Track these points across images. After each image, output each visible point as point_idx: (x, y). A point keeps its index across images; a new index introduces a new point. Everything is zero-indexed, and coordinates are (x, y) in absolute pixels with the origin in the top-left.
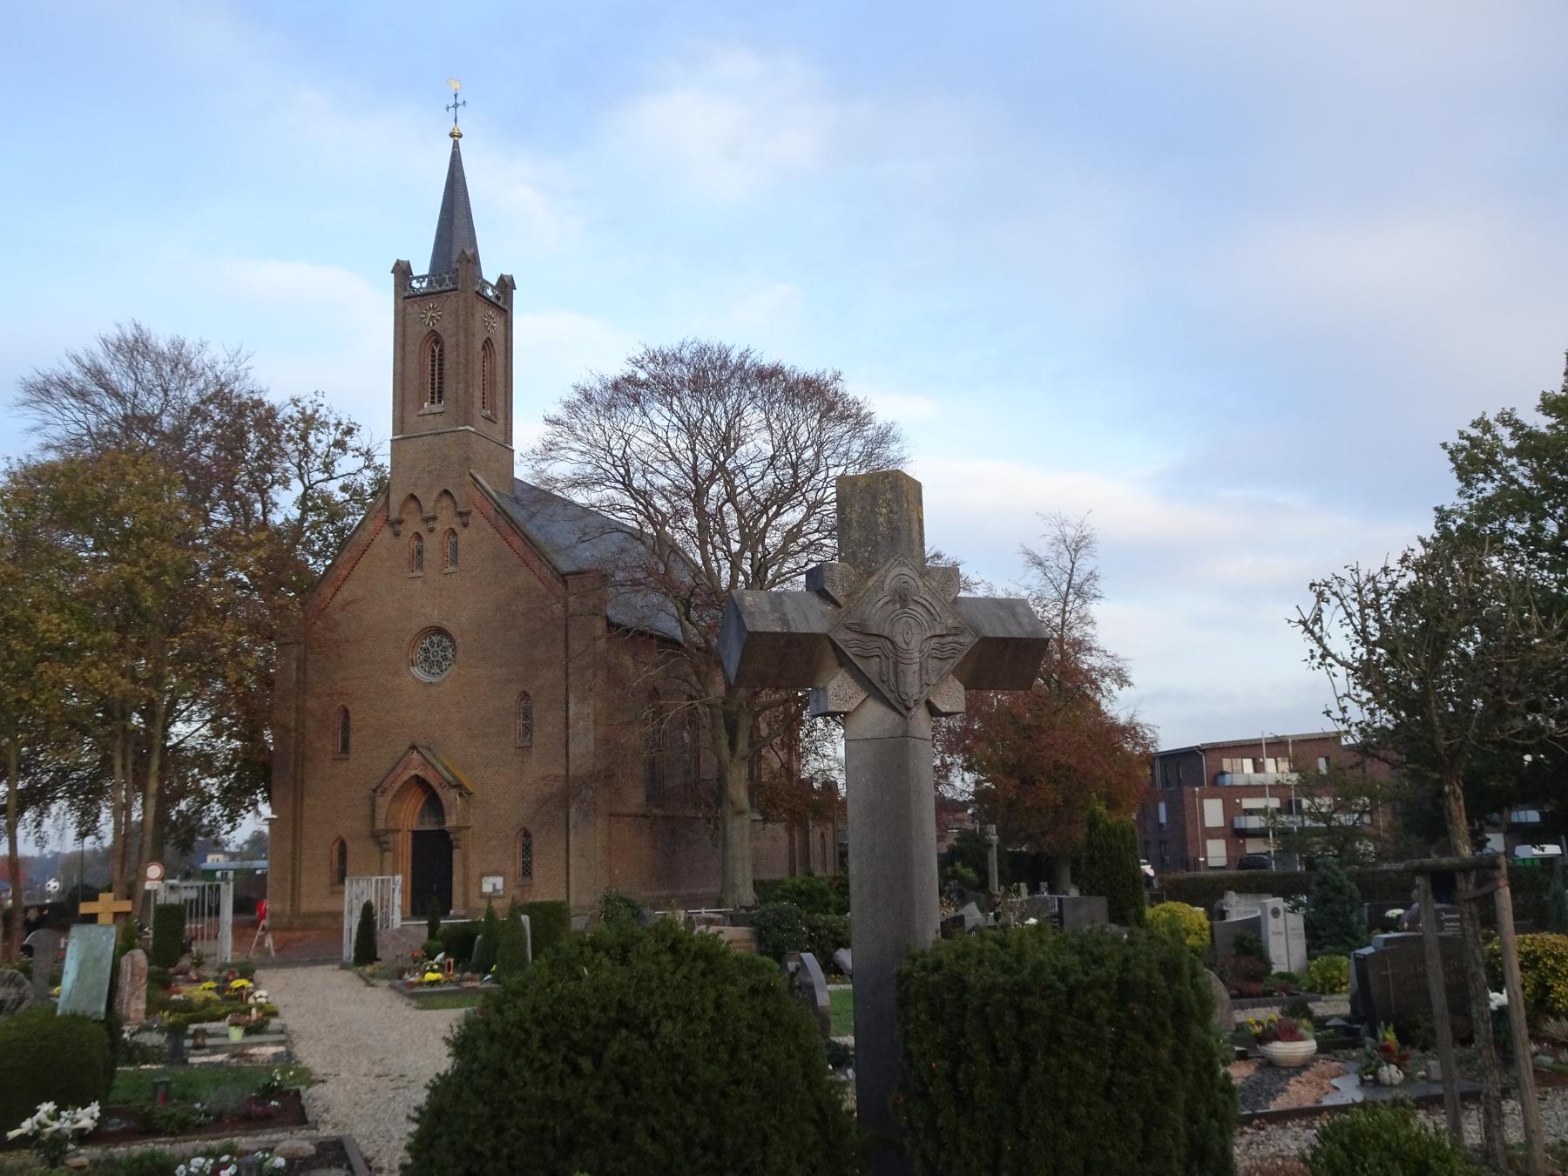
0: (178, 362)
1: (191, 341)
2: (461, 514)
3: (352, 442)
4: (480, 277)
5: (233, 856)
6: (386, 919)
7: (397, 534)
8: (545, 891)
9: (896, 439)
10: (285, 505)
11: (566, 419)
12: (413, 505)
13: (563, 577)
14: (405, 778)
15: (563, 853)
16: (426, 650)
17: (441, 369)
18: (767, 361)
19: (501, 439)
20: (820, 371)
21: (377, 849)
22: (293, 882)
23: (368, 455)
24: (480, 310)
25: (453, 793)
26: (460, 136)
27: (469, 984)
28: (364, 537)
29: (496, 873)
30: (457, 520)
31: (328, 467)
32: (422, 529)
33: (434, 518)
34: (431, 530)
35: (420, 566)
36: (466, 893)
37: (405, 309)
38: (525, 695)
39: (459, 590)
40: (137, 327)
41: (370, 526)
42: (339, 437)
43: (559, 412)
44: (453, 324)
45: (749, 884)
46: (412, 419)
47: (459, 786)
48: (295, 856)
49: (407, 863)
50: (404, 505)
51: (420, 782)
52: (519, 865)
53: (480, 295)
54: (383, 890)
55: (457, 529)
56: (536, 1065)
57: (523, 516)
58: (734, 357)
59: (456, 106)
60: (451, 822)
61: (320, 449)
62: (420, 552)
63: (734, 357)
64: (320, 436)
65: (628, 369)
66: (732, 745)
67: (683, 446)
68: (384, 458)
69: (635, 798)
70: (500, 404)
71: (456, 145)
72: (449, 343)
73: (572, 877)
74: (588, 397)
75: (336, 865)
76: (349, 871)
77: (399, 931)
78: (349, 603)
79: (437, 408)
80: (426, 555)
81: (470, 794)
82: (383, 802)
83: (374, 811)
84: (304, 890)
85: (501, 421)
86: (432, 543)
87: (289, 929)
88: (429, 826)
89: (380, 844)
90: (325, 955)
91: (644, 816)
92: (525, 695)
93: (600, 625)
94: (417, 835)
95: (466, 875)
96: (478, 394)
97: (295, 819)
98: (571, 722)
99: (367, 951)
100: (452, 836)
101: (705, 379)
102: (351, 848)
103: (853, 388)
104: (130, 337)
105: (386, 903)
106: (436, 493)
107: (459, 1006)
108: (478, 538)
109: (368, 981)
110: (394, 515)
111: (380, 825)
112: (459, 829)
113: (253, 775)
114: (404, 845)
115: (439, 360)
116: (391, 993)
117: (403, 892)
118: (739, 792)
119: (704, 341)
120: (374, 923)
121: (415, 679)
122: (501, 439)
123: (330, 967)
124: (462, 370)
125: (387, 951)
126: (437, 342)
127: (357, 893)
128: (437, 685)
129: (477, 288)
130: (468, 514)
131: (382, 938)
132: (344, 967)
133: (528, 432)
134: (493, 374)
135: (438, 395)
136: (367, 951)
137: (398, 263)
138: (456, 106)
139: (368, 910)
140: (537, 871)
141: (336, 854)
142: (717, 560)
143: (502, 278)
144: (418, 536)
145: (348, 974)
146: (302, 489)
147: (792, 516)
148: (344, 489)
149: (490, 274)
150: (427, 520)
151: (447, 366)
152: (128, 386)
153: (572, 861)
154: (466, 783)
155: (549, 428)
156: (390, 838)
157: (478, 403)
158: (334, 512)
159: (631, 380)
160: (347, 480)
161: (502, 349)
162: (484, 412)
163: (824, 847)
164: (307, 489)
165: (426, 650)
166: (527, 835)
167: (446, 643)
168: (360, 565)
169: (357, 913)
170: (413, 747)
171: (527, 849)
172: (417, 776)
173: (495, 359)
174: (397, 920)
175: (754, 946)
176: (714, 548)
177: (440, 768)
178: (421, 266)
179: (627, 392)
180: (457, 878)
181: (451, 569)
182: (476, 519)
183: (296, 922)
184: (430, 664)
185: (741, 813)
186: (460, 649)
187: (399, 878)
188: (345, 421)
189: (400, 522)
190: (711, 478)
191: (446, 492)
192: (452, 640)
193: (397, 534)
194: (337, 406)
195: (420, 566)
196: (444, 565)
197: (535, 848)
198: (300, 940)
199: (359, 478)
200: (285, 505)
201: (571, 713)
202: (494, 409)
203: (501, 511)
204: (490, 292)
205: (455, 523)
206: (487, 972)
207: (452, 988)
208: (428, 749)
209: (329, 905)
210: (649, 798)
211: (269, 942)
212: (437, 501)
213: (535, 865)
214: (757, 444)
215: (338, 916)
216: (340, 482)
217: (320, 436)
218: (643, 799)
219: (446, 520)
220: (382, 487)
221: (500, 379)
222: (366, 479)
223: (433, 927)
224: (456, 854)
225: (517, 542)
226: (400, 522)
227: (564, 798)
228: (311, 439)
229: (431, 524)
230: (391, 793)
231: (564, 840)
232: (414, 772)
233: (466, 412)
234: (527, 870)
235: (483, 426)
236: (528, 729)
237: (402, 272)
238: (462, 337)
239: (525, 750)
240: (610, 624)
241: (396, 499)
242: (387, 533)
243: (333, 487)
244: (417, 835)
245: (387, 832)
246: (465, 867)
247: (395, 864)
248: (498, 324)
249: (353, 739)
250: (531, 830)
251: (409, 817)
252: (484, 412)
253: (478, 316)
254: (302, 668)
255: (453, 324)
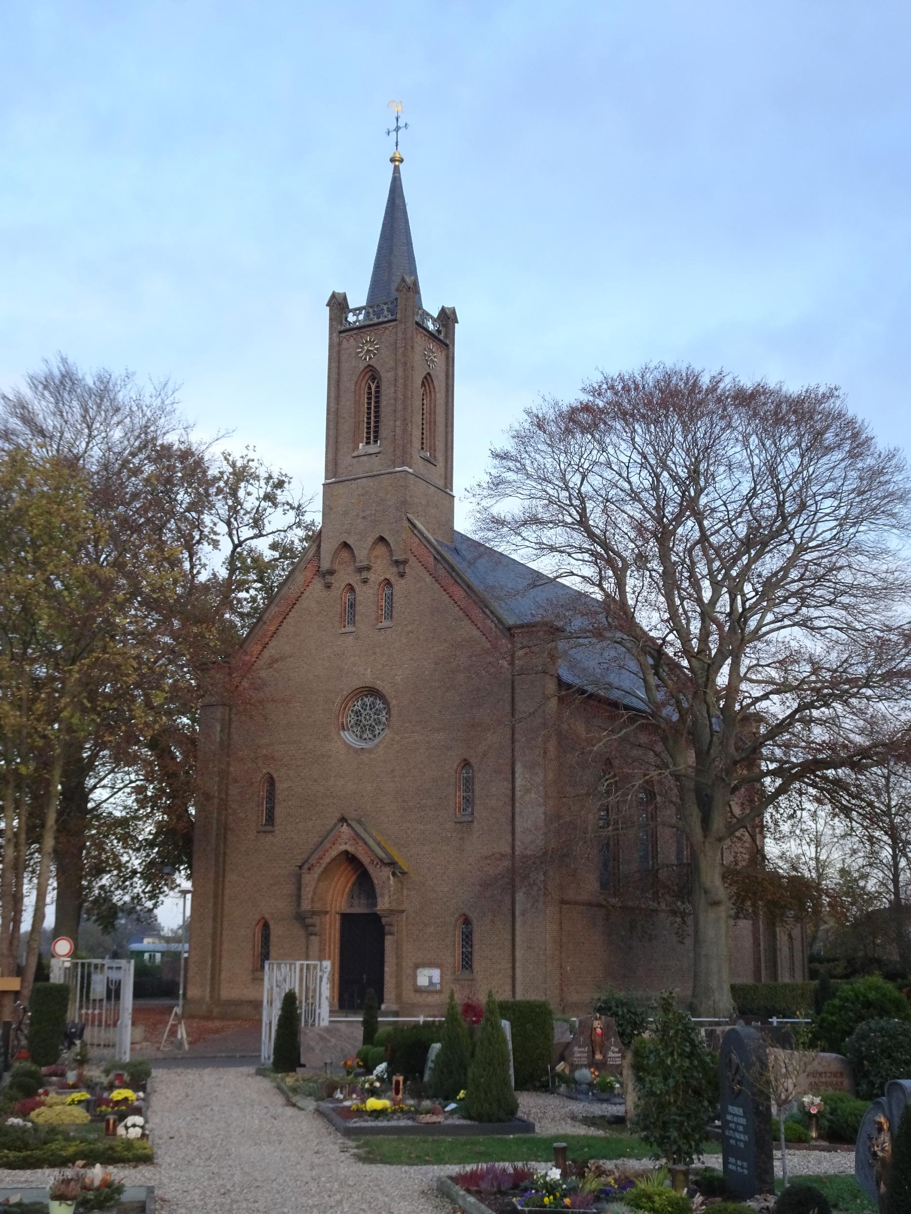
0: (102, 398)
1: (117, 372)
2: (397, 563)
3: (281, 496)
4: (420, 308)
5: (168, 940)
6: (312, 1013)
7: (328, 586)
8: (490, 985)
9: (899, 469)
10: (213, 562)
11: (513, 452)
12: (345, 554)
13: (509, 631)
14: (334, 853)
15: (508, 944)
16: (358, 713)
17: (377, 407)
18: (748, 383)
19: (441, 483)
20: (813, 385)
21: (302, 932)
22: (213, 966)
23: (299, 510)
24: (420, 341)
25: (387, 872)
26: (401, 161)
27: (429, 1118)
28: (292, 590)
29: (431, 965)
30: (394, 570)
31: (257, 522)
32: (355, 580)
33: (368, 568)
34: (365, 581)
35: (353, 621)
36: (399, 985)
37: (340, 344)
38: (466, 764)
39: (397, 649)
40: (64, 361)
41: (300, 578)
42: (269, 489)
43: (507, 445)
44: (389, 363)
45: (726, 988)
46: (346, 461)
47: (392, 864)
48: (216, 937)
49: (334, 947)
50: (336, 554)
51: (350, 859)
52: (458, 957)
53: (420, 326)
54: (308, 977)
55: (393, 580)
56: (25, 704)
57: (462, 570)
58: (705, 381)
59: (397, 129)
60: (383, 904)
61: (250, 503)
62: (352, 605)
63: (705, 381)
64: (250, 489)
65: (585, 398)
66: (706, 822)
67: (647, 484)
68: (315, 515)
69: (589, 885)
70: (440, 445)
71: (396, 170)
72: (386, 377)
73: (518, 972)
74: (540, 424)
75: (258, 949)
76: (273, 954)
77: (327, 1030)
78: (277, 661)
79: (372, 449)
80: (359, 608)
81: (403, 873)
82: (310, 879)
83: (299, 889)
84: (224, 975)
85: (441, 464)
86: (366, 595)
87: (208, 1017)
88: (360, 909)
89: (306, 927)
90: (238, 1055)
91: (600, 906)
92: (466, 764)
93: (551, 686)
94: (345, 917)
95: (399, 965)
96: (417, 433)
97: (216, 896)
98: (518, 794)
99: (288, 1056)
100: (384, 920)
101: (670, 403)
102: (276, 930)
103: (856, 405)
104: (56, 372)
105: (311, 993)
106: (370, 540)
107: (420, 1160)
108: (416, 589)
109: (289, 1097)
110: (325, 565)
111: (306, 906)
112: (391, 912)
113: (177, 847)
114: (332, 929)
115: (375, 398)
116: (319, 1124)
117: (332, 981)
118: (712, 879)
119: (669, 365)
120: (297, 1018)
121: (349, 747)
122: (441, 483)
123: (245, 1070)
124: (400, 407)
125: (313, 1052)
126: (373, 378)
127: (280, 978)
128: (370, 751)
129: (417, 319)
130: (405, 562)
131: (307, 1038)
132: (261, 1072)
133: (471, 466)
134: (433, 412)
135: (374, 434)
136: (288, 1056)
137: (334, 295)
138: (397, 129)
139: (290, 1000)
140: (478, 964)
141: (258, 936)
142: (685, 612)
143: (443, 311)
144: (351, 588)
145: (265, 1084)
146: (231, 547)
147: (770, 564)
148: (274, 546)
149: (431, 305)
150: (360, 570)
151: (383, 403)
152: (50, 423)
153: (518, 954)
154: (401, 862)
155: (496, 462)
156: (316, 920)
157: (417, 444)
158: (261, 567)
159: (586, 408)
160: (277, 538)
161: (443, 385)
162: (422, 454)
163: (791, 949)
164: (235, 547)
165: (358, 713)
166: (467, 922)
167: (379, 705)
168: (289, 620)
169: (278, 1004)
170: (343, 820)
171: (467, 938)
172: (346, 852)
173: (437, 392)
174: (324, 1014)
175: (846, 1082)
176: (682, 599)
177: (371, 842)
178: (358, 298)
179: (583, 420)
180: (389, 969)
181: (385, 623)
182: (414, 569)
183: (216, 1011)
184: (364, 729)
185: (716, 903)
186: (394, 711)
187: (327, 964)
188: (275, 475)
189: (331, 572)
190: (679, 519)
191: (382, 539)
192: (386, 702)
193: (328, 586)
194: (270, 460)
195: (353, 621)
196: (378, 619)
197: (476, 936)
198: (217, 1031)
199: (290, 534)
200: (213, 562)
201: (519, 782)
202: (433, 449)
203: (440, 558)
204: (431, 326)
205: (391, 573)
206: (450, 1097)
207: (403, 1123)
208: (359, 822)
209: (249, 993)
210: (604, 885)
211: (182, 1032)
212: (372, 548)
213: (476, 957)
214: (730, 486)
215: (257, 1005)
216: (269, 540)
217: (250, 489)
218: (596, 886)
219: (381, 570)
220: (315, 539)
221: (440, 410)
222: (296, 536)
223: (370, 1027)
224: (389, 941)
225: (459, 593)
226: (331, 572)
227: (509, 881)
228: (241, 494)
229: (365, 575)
230: (318, 870)
231: (509, 928)
232: (343, 847)
233: (404, 452)
234: (467, 962)
235: (420, 466)
236: (469, 801)
237: (338, 304)
238: (400, 372)
239: (465, 825)
240: (561, 684)
241: (328, 547)
242: (317, 585)
243: (262, 546)
244: (345, 917)
245: (314, 913)
246: (398, 957)
247: (322, 950)
248: (439, 358)
249: (279, 812)
250: (473, 916)
251: (336, 897)
252: (422, 454)
253: (418, 349)
254: (227, 726)
255: (389, 363)
